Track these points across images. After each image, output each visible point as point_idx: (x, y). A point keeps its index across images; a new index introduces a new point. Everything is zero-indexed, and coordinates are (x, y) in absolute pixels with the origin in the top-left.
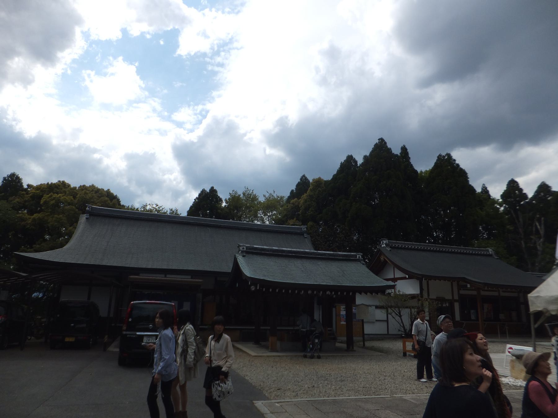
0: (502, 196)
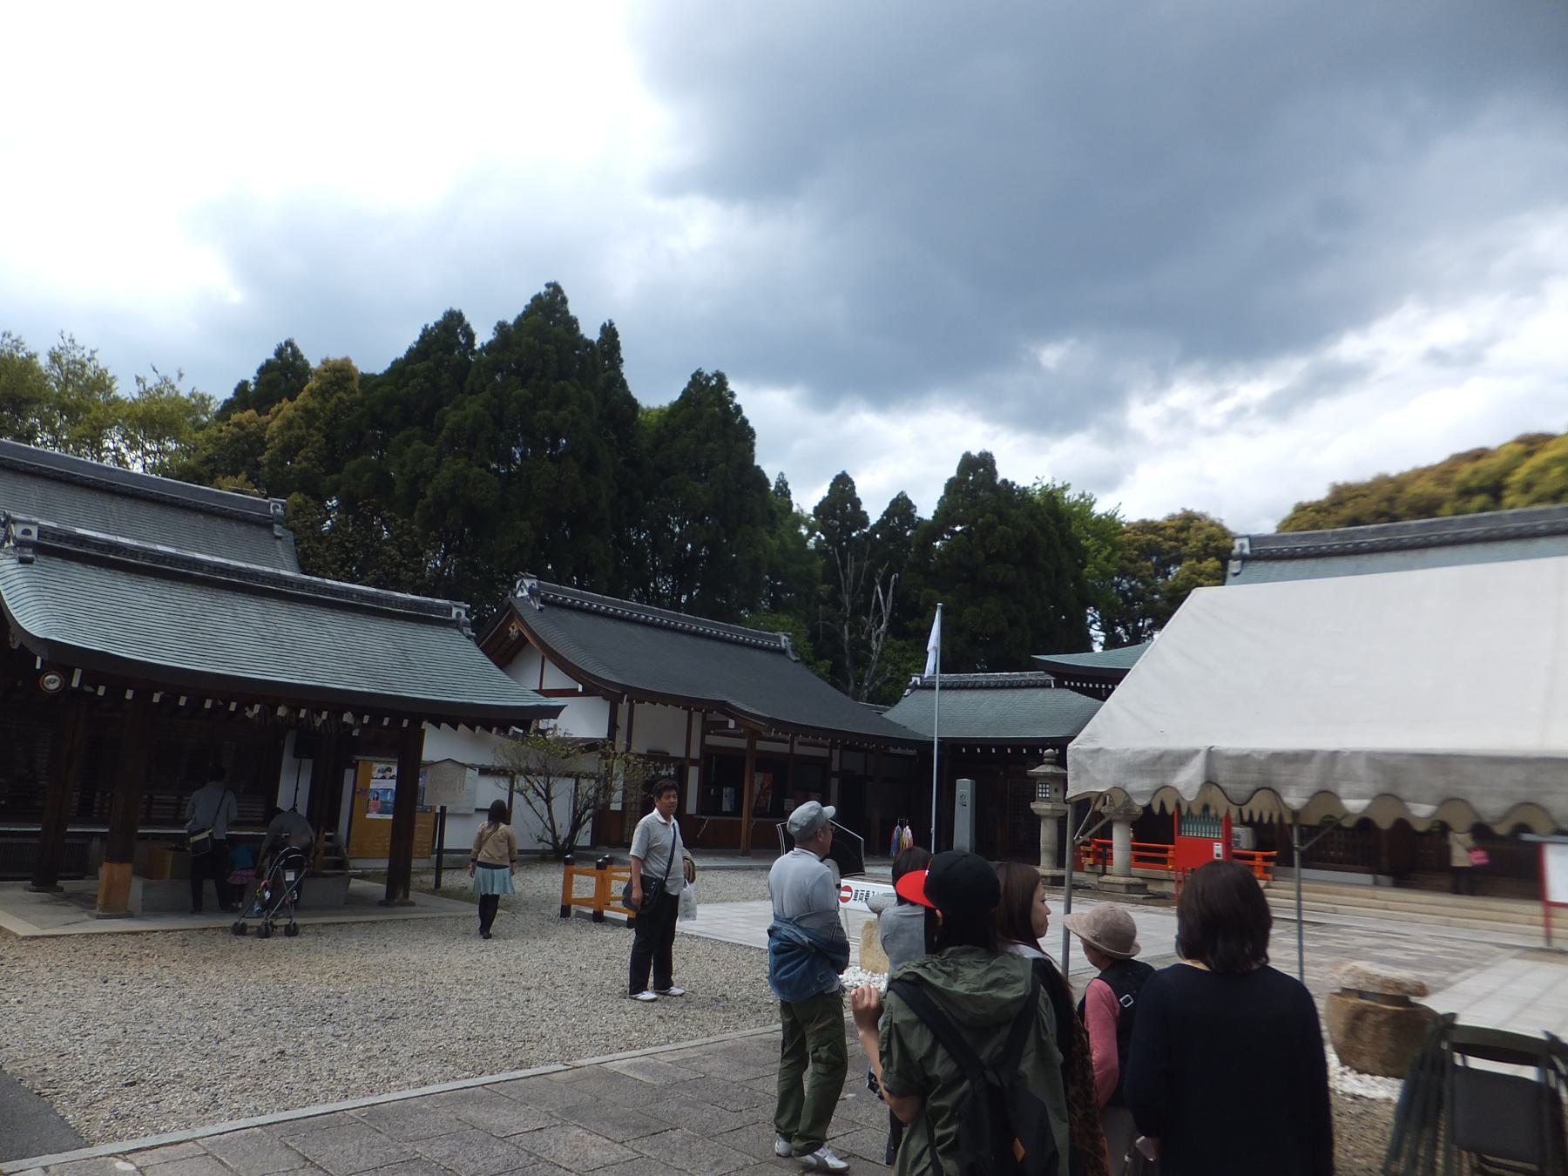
0: (818, 511)
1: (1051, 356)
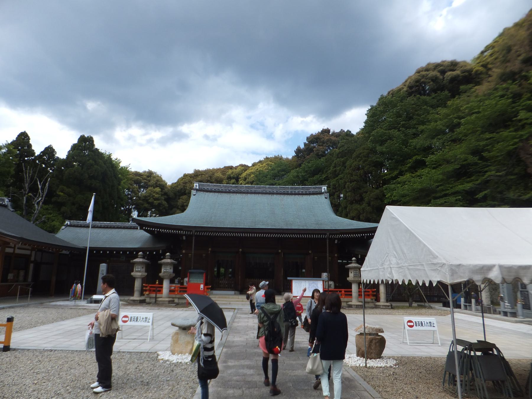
1: (91, 105)
